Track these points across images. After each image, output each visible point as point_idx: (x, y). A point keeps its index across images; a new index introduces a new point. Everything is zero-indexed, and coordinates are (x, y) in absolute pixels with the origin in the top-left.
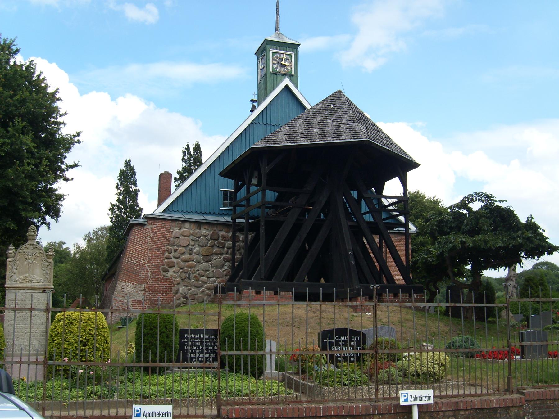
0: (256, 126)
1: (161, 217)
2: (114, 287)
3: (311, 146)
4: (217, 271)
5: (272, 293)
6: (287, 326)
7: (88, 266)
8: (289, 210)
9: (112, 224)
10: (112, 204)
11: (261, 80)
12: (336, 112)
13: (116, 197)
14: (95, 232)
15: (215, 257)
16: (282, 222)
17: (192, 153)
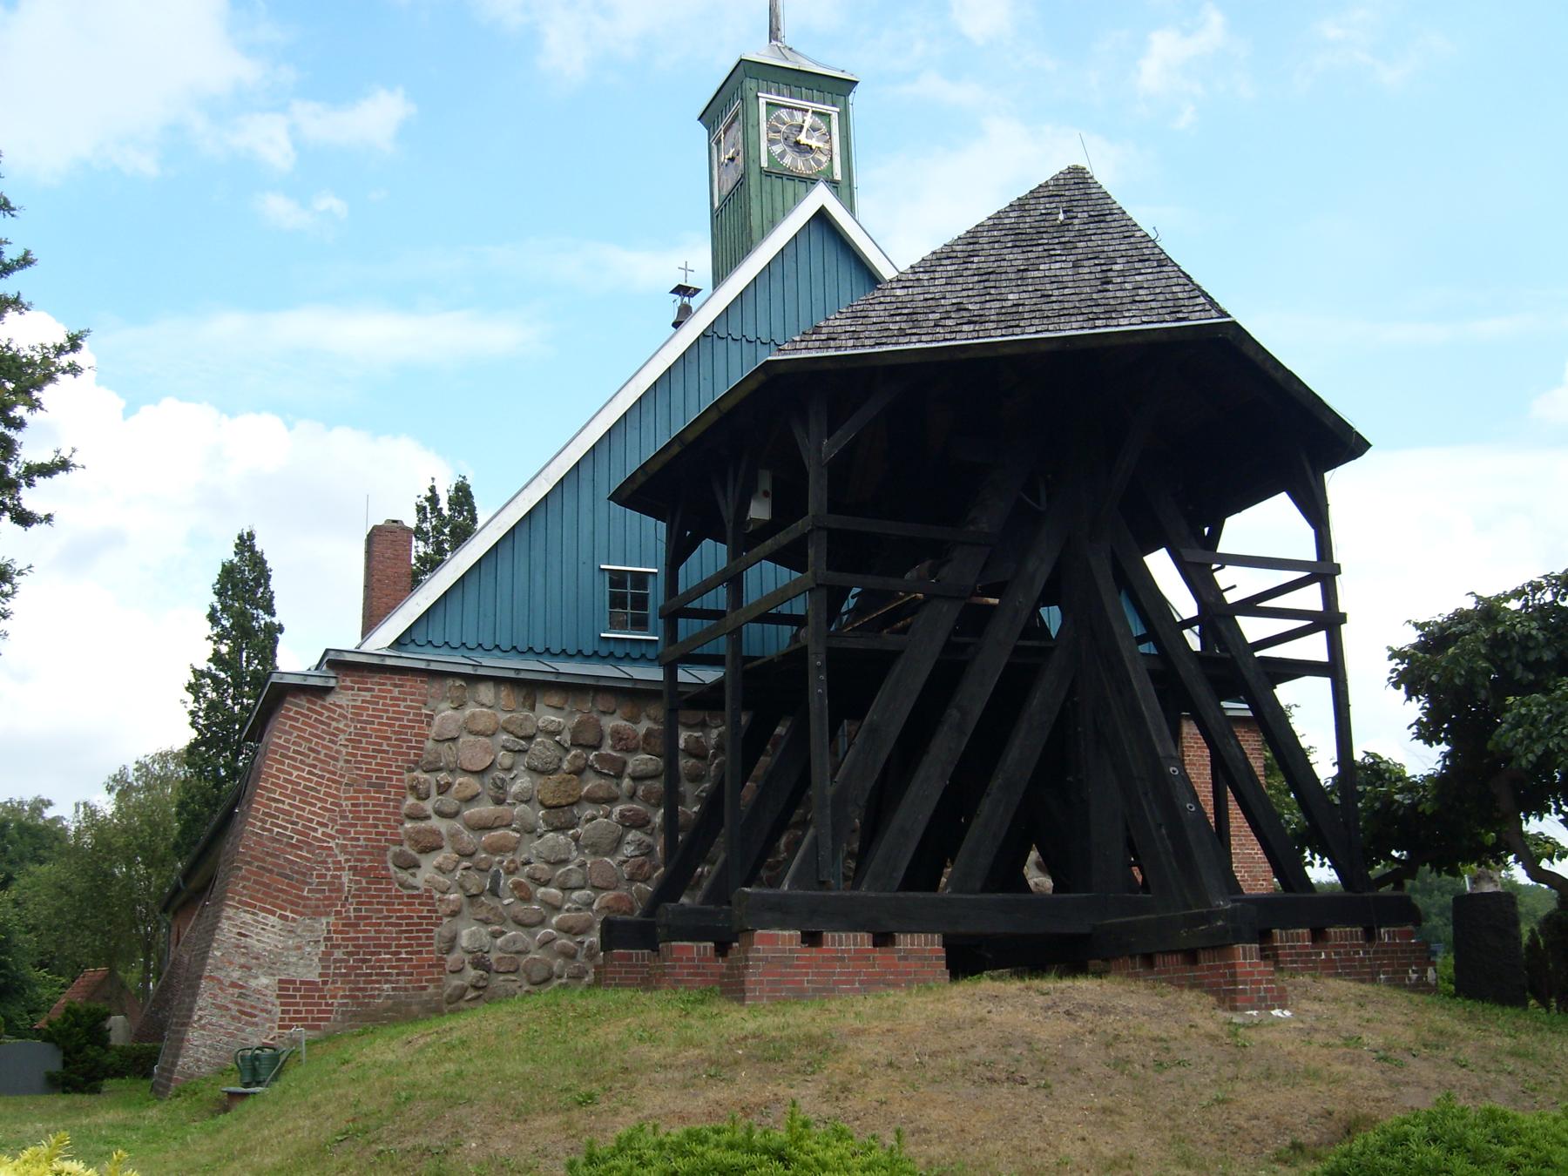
0: (720, 346)
1: (389, 662)
2: (213, 928)
3: (1007, 351)
4: (600, 860)
5: (864, 939)
6: (992, 1080)
7: (120, 870)
8: (913, 608)
9: (194, 734)
10: (195, 671)
11: (726, 201)
12: (1081, 234)
13: (208, 649)
14: (141, 766)
15: (589, 813)
16: (896, 654)
17: (446, 512)
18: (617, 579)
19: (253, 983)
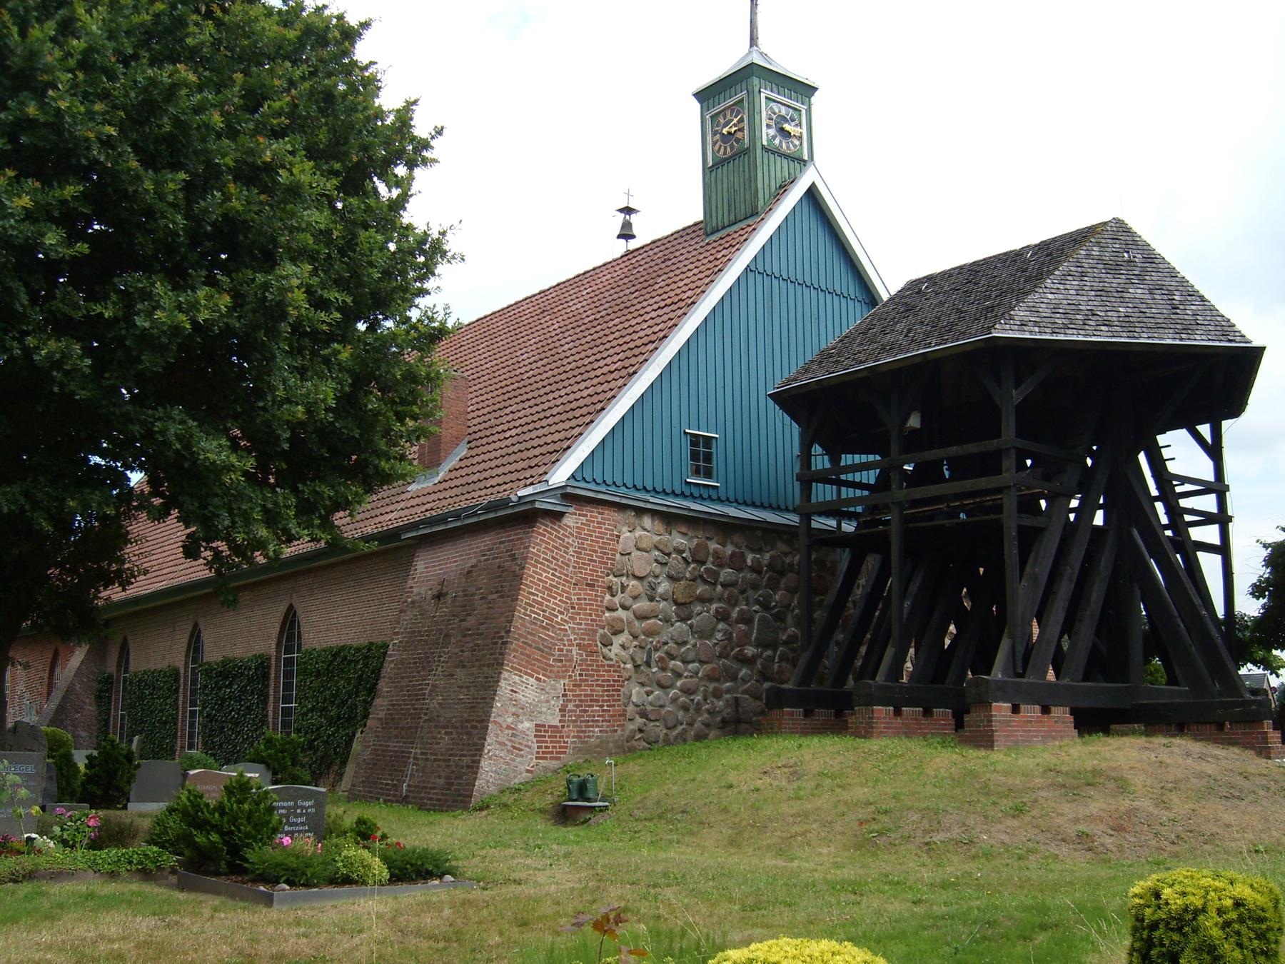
18: (695, 440)
19: (520, 726)
